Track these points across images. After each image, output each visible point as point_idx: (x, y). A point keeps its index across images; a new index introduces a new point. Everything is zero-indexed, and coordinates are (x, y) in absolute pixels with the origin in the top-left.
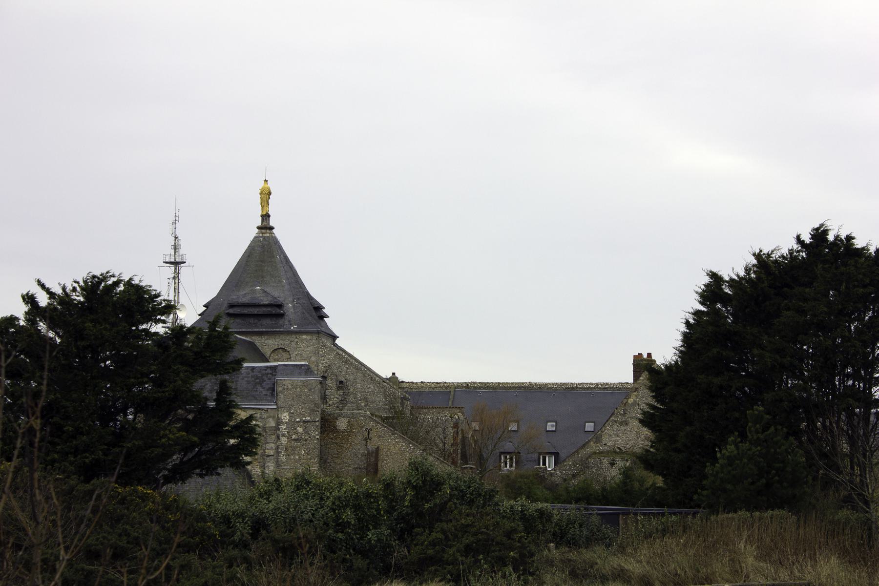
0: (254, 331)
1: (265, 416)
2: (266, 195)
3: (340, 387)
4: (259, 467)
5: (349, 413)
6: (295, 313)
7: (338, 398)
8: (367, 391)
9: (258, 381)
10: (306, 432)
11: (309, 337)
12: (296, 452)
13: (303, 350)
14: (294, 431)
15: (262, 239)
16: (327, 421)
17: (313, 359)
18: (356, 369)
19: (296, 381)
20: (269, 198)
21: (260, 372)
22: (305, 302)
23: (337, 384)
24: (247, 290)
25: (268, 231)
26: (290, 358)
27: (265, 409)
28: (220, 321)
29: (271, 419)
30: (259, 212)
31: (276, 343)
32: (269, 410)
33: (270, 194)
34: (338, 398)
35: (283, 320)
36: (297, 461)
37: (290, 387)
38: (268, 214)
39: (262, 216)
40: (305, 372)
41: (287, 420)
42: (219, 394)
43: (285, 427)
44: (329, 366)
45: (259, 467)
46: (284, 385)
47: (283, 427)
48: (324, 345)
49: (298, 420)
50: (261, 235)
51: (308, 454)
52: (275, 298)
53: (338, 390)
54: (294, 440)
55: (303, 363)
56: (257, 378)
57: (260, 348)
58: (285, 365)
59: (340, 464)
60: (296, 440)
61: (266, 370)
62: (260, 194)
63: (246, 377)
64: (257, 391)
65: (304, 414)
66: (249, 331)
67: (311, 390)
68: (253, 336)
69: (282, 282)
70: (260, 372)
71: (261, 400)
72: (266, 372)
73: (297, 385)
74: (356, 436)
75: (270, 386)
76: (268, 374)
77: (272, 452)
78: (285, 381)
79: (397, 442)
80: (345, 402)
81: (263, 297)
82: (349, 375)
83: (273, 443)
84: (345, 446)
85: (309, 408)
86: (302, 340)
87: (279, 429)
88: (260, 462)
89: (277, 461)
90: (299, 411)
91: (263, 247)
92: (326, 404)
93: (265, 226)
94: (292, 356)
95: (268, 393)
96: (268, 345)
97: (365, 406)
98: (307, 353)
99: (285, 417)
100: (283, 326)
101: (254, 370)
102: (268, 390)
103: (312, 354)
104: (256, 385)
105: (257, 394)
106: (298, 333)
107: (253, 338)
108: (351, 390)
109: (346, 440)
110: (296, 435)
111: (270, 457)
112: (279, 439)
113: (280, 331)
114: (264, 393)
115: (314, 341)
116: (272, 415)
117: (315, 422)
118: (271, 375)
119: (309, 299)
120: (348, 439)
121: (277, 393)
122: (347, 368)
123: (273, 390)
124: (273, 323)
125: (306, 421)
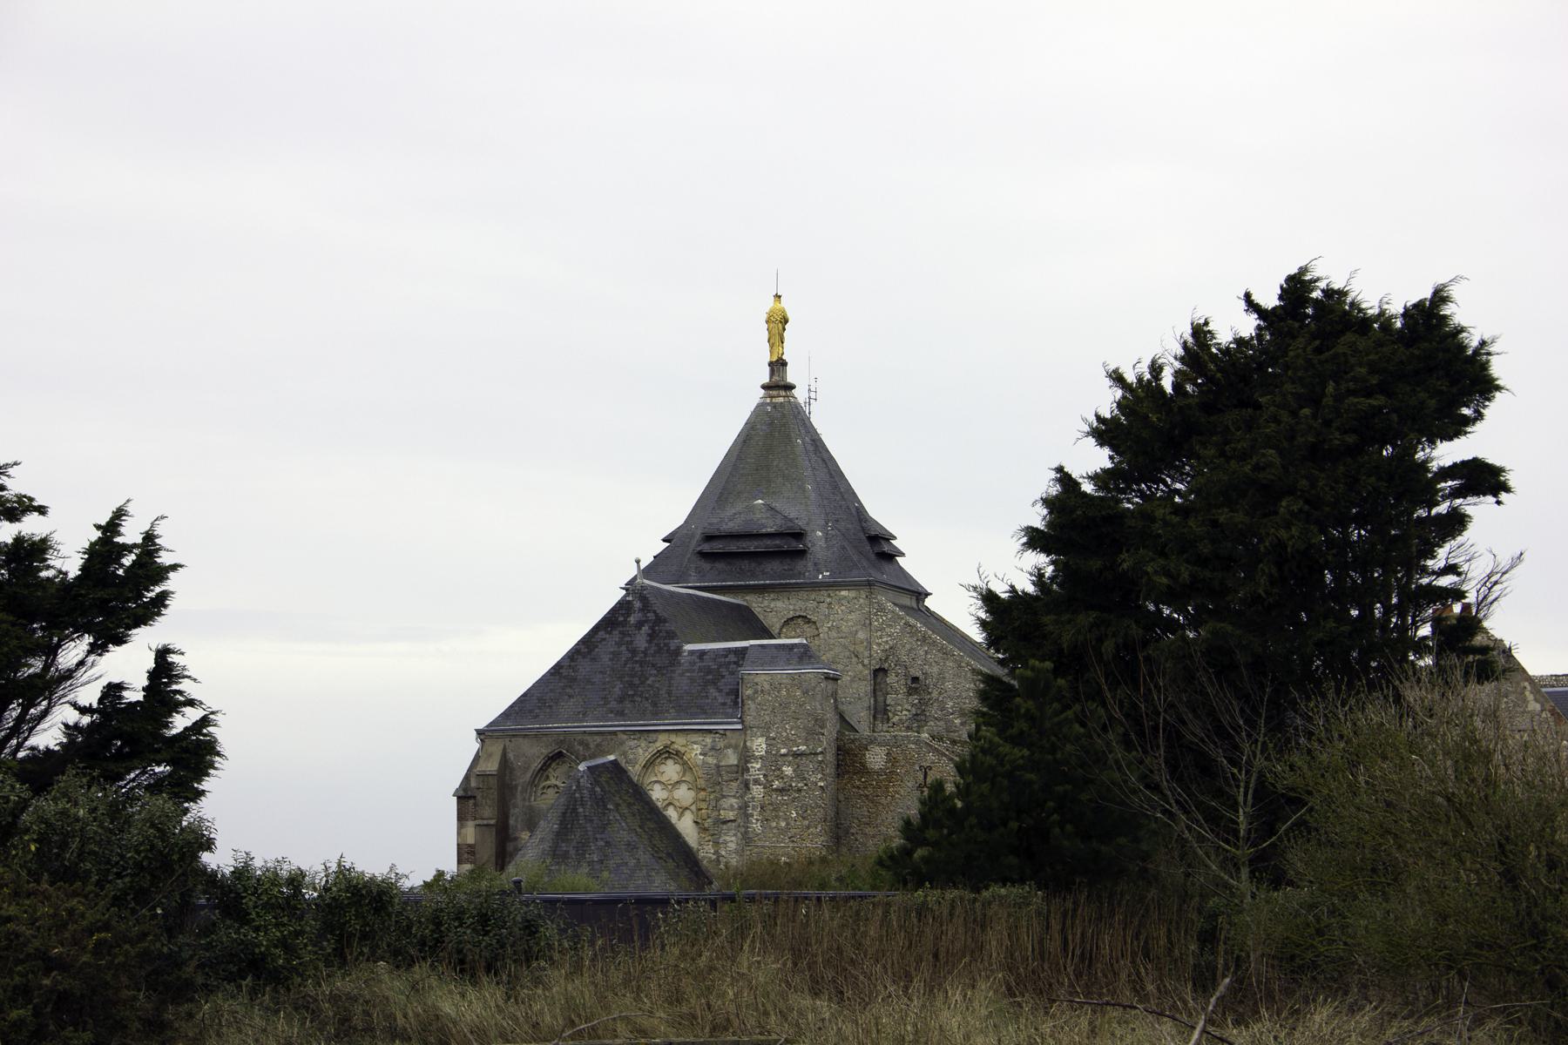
0: (749, 585)
1: (721, 744)
2: (778, 324)
3: (913, 688)
4: (711, 843)
6: (828, 548)
7: (909, 711)
8: (964, 695)
9: (710, 677)
10: (799, 774)
11: (852, 594)
12: (781, 814)
13: (842, 619)
15: (769, 408)
17: (861, 635)
19: (779, 676)
20: (784, 329)
22: (850, 526)
23: (906, 684)
24: (739, 506)
26: (819, 635)
27: (721, 732)
28: (123, 523)
30: (766, 357)
31: (791, 607)
33: (786, 321)
34: (909, 711)
35: (804, 562)
36: (783, 831)
37: (767, 687)
39: (771, 364)
40: (799, 658)
41: (763, 753)
42: (154, 675)
43: (758, 766)
44: (891, 648)
45: (711, 843)
46: (757, 684)
47: (754, 765)
48: (882, 609)
49: (783, 751)
50: (768, 400)
51: (804, 818)
52: (791, 520)
53: (911, 695)
54: (776, 790)
55: (796, 641)
56: (709, 671)
57: (761, 617)
59: (874, 836)
61: (726, 656)
62: (767, 322)
63: (688, 671)
64: (707, 697)
65: (795, 741)
66: (741, 586)
67: (807, 692)
68: (747, 593)
69: (804, 491)
71: (714, 714)
72: (727, 660)
75: (732, 687)
76: (729, 663)
77: (731, 815)
78: (758, 676)
80: (923, 718)
83: (734, 797)
84: (883, 801)
85: (804, 728)
86: (840, 599)
87: (748, 770)
89: (746, 832)
90: (785, 734)
91: (771, 424)
92: (888, 723)
93: (778, 384)
94: (821, 630)
95: (728, 701)
96: (776, 611)
97: (962, 724)
98: (849, 624)
99: (759, 745)
100: (804, 574)
101: (705, 657)
102: (728, 694)
103: (859, 627)
104: (706, 686)
105: (708, 704)
106: (832, 586)
107: (747, 598)
108: (935, 695)
109: (883, 789)
110: (780, 780)
111: (730, 824)
112: (749, 790)
113: (797, 583)
115: (861, 601)
116: (733, 742)
118: (735, 666)
119: (860, 521)
120: (887, 788)
121: (742, 701)
122: (926, 652)
123: (735, 699)
124: (786, 568)
125: (798, 753)
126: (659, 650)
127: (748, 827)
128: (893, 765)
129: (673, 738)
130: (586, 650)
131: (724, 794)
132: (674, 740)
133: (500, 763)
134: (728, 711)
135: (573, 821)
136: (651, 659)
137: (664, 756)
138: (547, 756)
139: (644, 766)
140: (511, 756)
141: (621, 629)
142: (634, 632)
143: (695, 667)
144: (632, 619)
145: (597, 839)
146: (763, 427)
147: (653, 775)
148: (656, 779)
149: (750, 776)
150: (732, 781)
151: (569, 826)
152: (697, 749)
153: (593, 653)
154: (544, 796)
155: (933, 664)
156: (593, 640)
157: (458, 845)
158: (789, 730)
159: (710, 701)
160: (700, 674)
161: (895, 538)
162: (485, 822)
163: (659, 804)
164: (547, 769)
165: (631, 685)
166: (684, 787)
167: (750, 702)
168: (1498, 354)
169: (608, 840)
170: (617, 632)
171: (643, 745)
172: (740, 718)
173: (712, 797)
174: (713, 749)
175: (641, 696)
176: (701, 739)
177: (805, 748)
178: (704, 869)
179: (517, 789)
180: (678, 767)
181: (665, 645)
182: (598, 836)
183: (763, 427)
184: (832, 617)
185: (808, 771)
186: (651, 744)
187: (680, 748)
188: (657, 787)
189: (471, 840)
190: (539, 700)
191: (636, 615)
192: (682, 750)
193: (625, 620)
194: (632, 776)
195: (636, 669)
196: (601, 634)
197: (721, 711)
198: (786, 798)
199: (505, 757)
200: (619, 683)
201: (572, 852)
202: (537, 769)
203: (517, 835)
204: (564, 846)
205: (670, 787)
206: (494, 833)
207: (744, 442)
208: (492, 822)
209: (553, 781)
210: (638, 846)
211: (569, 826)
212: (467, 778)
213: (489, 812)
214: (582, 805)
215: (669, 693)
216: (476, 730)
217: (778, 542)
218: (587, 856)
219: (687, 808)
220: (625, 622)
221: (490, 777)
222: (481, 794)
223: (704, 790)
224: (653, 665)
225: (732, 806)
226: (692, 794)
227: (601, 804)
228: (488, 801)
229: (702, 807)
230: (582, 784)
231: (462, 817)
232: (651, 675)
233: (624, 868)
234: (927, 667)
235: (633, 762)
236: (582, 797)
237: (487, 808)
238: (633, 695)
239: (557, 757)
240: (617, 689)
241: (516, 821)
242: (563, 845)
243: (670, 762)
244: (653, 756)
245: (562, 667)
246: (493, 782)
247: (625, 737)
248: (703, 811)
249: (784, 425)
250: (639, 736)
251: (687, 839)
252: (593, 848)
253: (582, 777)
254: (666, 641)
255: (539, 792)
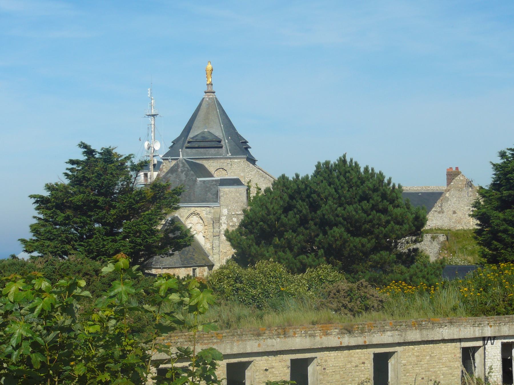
14: (231, 220)
49: (233, 213)
95: (214, 197)
129: (196, 208)
152: (204, 212)
161: (248, 142)
168: (115, 148)
174: (210, 212)
181: (191, 178)
184: (232, 169)
192: (199, 213)
225: (217, 231)
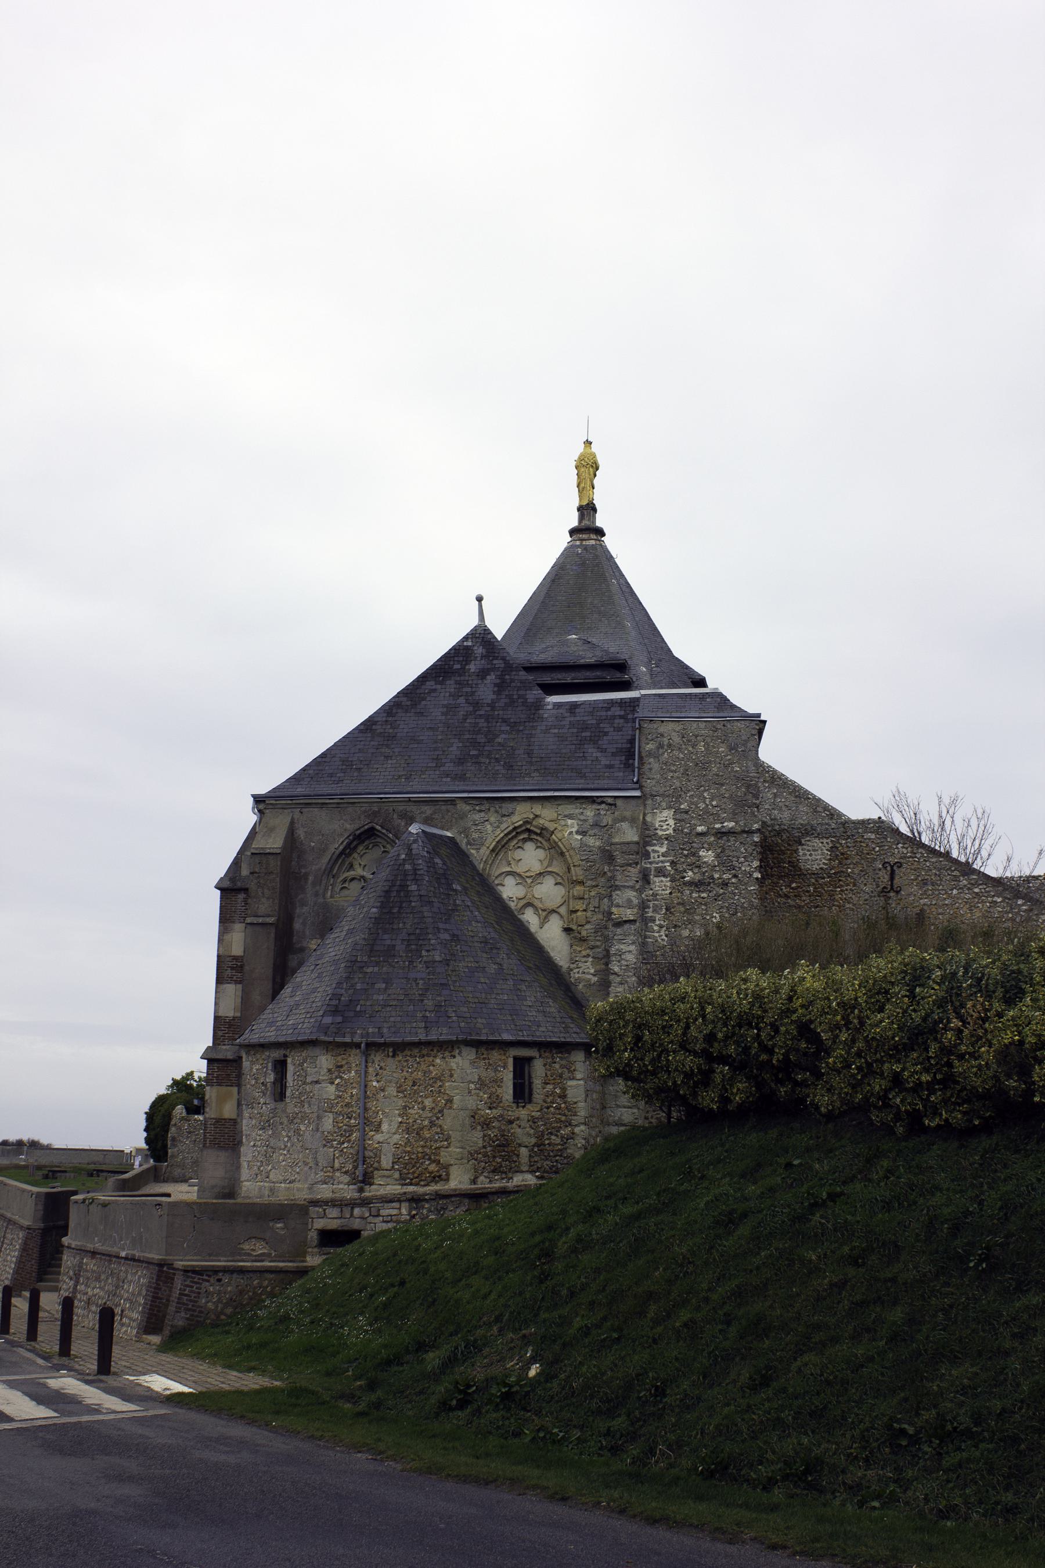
4: (590, 959)
5: (833, 826)
9: (588, 734)
10: (725, 861)
12: (697, 918)
14: (693, 859)
16: (771, 851)
18: (796, 797)
20: (595, 475)
21: (591, 713)
25: (593, 536)
27: (610, 801)
29: (625, 825)
30: (575, 501)
32: (619, 802)
33: (597, 469)
37: (676, 739)
38: (593, 503)
39: (580, 509)
41: (671, 831)
43: (664, 850)
45: (590, 959)
47: (657, 848)
50: (578, 543)
56: (585, 727)
58: (660, 695)
60: (696, 886)
61: (608, 709)
64: (584, 758)
70: (591, 713)
72: (609, 713)
73: (696, 736)
74: (855, 885)
75: (620, 746)
76: (614, 717)
77: (629, 914)
79: (977, 893)
81: (584, 650)
82: (780, 809)
83: (632, 887)
85: (731, 797)
87: (647, 855)
88: (592, 948)
90: (702, 806)
91: (583, 564)
99: (664, 821)
101: (577, 710)
102: (613, 754)
110: (696, 870)
111: (627, 926)
112: (649, 883)
114: (604, 761)
116: (628, 814)
117: (750, 832)
118: (622, 721)
120: (831, 895)
121: (641, 758)
122: (775, 795)
125: (724, 830)
126: (512, 703)
127: (646, 937)
128: (840, 863)
129: (538, 809)
130: (409, 703)
131: (617, 883)
132: (538, 813)
133: (286, 838)
134: (616, 774)
135: (401, 902)
136: (501, 712)
137: (522, 837)
138: (352, 833)
139: (493, 850)
140: (301, 833)
141: (458, 679)
142: (475, 682)
143: (563, 723)
144: (472, 667)
145: (438, 928)
146: (575, 568)
147: (504, 862)
148: (509, 869)
149: (651, 863)
150: (630, 865)
151: (395, 910)
152: (573, 825)
153: (418, 706)
154: (345, 892)
155: (784, 809)
156: (418, 691)
157: (219, 956)
158: (708, 800)
159: (589, 762)
160: (571, 730)
162: (260, 920)
163: (512, 905)
164: (350, 854)
165: (475, 743)
166: (549, 882)
167: (652, 760)
169: (456, 932)
170: (452, 682)
171: (492, 819)
172: (637, 783)
173: (593, 894)
174: (596, 825)
175: (488, 757)
176: (577, 811)
177: (732, 824)
178: (579, 996)
179: (306, 879)
180: (541, 854)
182: (441, 926)
183: (575, 568)
185: (738, 858)
186: (505, 819)
187: (547, 824)
188: (510, 881)
189: (237, 950)
190: (343, 761)
191: (477, 662)
192: (551, 826)
193: (463, 668)
194: (476, 864)
195: (481, 725)
196: (430, 684)
197: (606, 774)
198: (704, 895)
199: (293, 834)
200: (457, 741)
201: (400, 947)
202: (338, 852)
203: (304, 944)
204: (387, 940)
205: (529, 881)
206: (273, 935)
207: (553, 581)
208: (271, 920)
209: (359, 871)
210: (498, 946)
211: (395, 910)
212: (236, 863)
213: (265, 907)
214: (415, 880)
215: (530, 754)
216: (253, 796)
217: (598, 673)
218: (424, 953)
219: (553, 911)
220: (462, 671)
221: (271, 857)
222: (255, 881)
223: (582, 883)
224: (504, 721)
225: (629, 901)
226: (561, 891)
227: (443, 881)
228: (266, 891)
229: (577, 908)
230: (414, 852)
231: (226, 918)
232: (503, 732)
233: (481, 974)
234: (776, 812)
235: (479, 844)
236: (415, 870)
237: (264, 900)
238: (477, 756)
239: (365, 837)
240: (454, 748)
241: (304, 924)
242: (386, 937)
243: (529, 846)
244: (506, 835)
245: (375, 723)
246: (275, 864)
247: (468, 808)
248: (579, 913)
249: (597, 565)
250: (487, 806)
251: (552, 954)
252: (433, 942)
253: (415, 841)
254: (521, 692)
255: (337, 889)
